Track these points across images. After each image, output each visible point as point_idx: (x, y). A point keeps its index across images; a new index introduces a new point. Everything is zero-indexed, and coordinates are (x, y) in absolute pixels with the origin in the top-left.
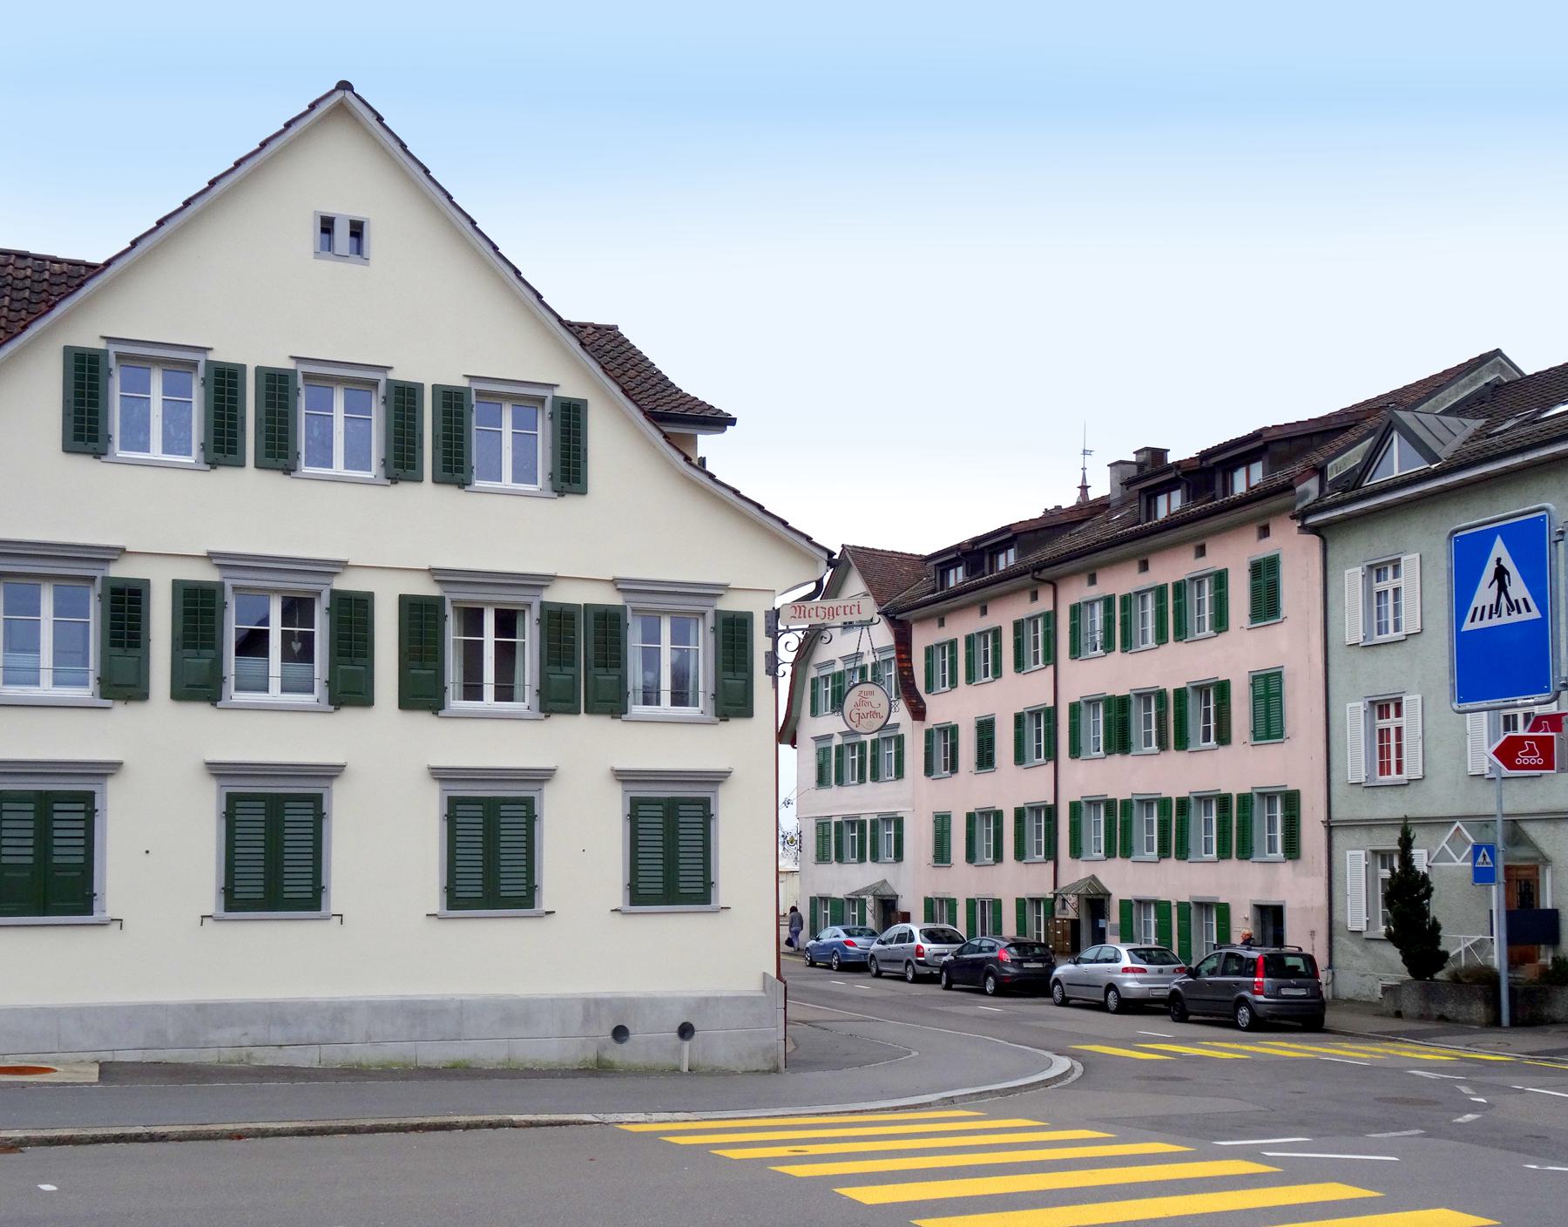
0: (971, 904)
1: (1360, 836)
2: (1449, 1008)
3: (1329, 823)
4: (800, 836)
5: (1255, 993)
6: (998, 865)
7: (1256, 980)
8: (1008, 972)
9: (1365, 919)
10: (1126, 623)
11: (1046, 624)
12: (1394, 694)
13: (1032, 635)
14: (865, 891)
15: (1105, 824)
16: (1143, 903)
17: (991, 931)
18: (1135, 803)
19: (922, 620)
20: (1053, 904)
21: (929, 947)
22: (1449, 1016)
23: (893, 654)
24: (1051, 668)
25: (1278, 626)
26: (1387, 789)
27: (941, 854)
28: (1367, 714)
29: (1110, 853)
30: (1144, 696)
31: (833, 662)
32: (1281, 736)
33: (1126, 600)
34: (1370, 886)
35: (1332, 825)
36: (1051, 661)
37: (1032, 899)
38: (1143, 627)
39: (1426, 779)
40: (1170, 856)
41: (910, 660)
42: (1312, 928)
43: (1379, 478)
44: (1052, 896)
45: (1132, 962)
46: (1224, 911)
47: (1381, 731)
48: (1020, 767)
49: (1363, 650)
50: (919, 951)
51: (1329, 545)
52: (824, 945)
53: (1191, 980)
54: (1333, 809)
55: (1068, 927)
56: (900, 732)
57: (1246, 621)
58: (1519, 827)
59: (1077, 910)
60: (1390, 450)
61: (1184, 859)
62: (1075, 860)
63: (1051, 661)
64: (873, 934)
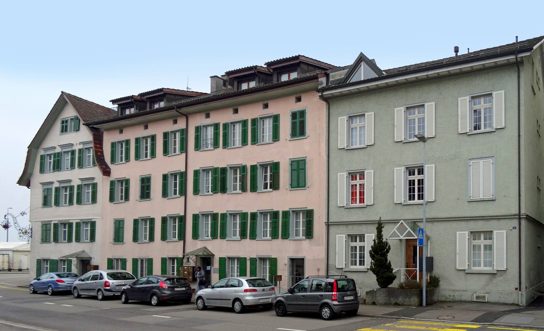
0: (135, 261)
1: (343, 228)
2: (400, 300)
3: (328, 223)
4: (32, 230)
5: (333, 300)
6: (151, 243)
7: (333, 293)
8: (165, 293)
9: (344, 263)
10: (225, 136)
11: (182, 134)
12: (360, 170)
13: (173, 140)
14: (71, 256)
15: (149, 229)
16: (232, 259)
17: (147, 273)
18: (228, 215)
19: (108, 130)
20: (182, 260)
21: (111, 282)
22: (400, 303)
23: (92, 145)
24: (184, 155)
25: (304, 140)
26: (356, 209)
27: (118, 237)
28: (348, 178)
29: (214, 236)
30: (234, 169)
31: (55, 148)
32: (305, 186)
33: (225, 126)
34: (347, 250)
35: (329, 224)
36: (184, 151)
37: (170, 258)
38: (234, 138)
39: (374, 205)
40: (246, 238)
41: (102, 148)
42: (318, 268)
43: (354, 79)
44: (182, 256)
45: (250, 286)
46: (273, 262)
47: (352, 186)
48: (165, 199)
49: (346, 151)
50: (106, 284)
51: (331, 107)
52: (43, 282)
53: (290, 294)
54: (330, 218)
55: (191, 270)
56: (95, 181)
57: (289, 137)
58: (417, 225)
59: (196, 263)
60: (360, 67)
61: (254, 239)
62: (195, 241)
63: (184, 151)
64: (76, 276)
